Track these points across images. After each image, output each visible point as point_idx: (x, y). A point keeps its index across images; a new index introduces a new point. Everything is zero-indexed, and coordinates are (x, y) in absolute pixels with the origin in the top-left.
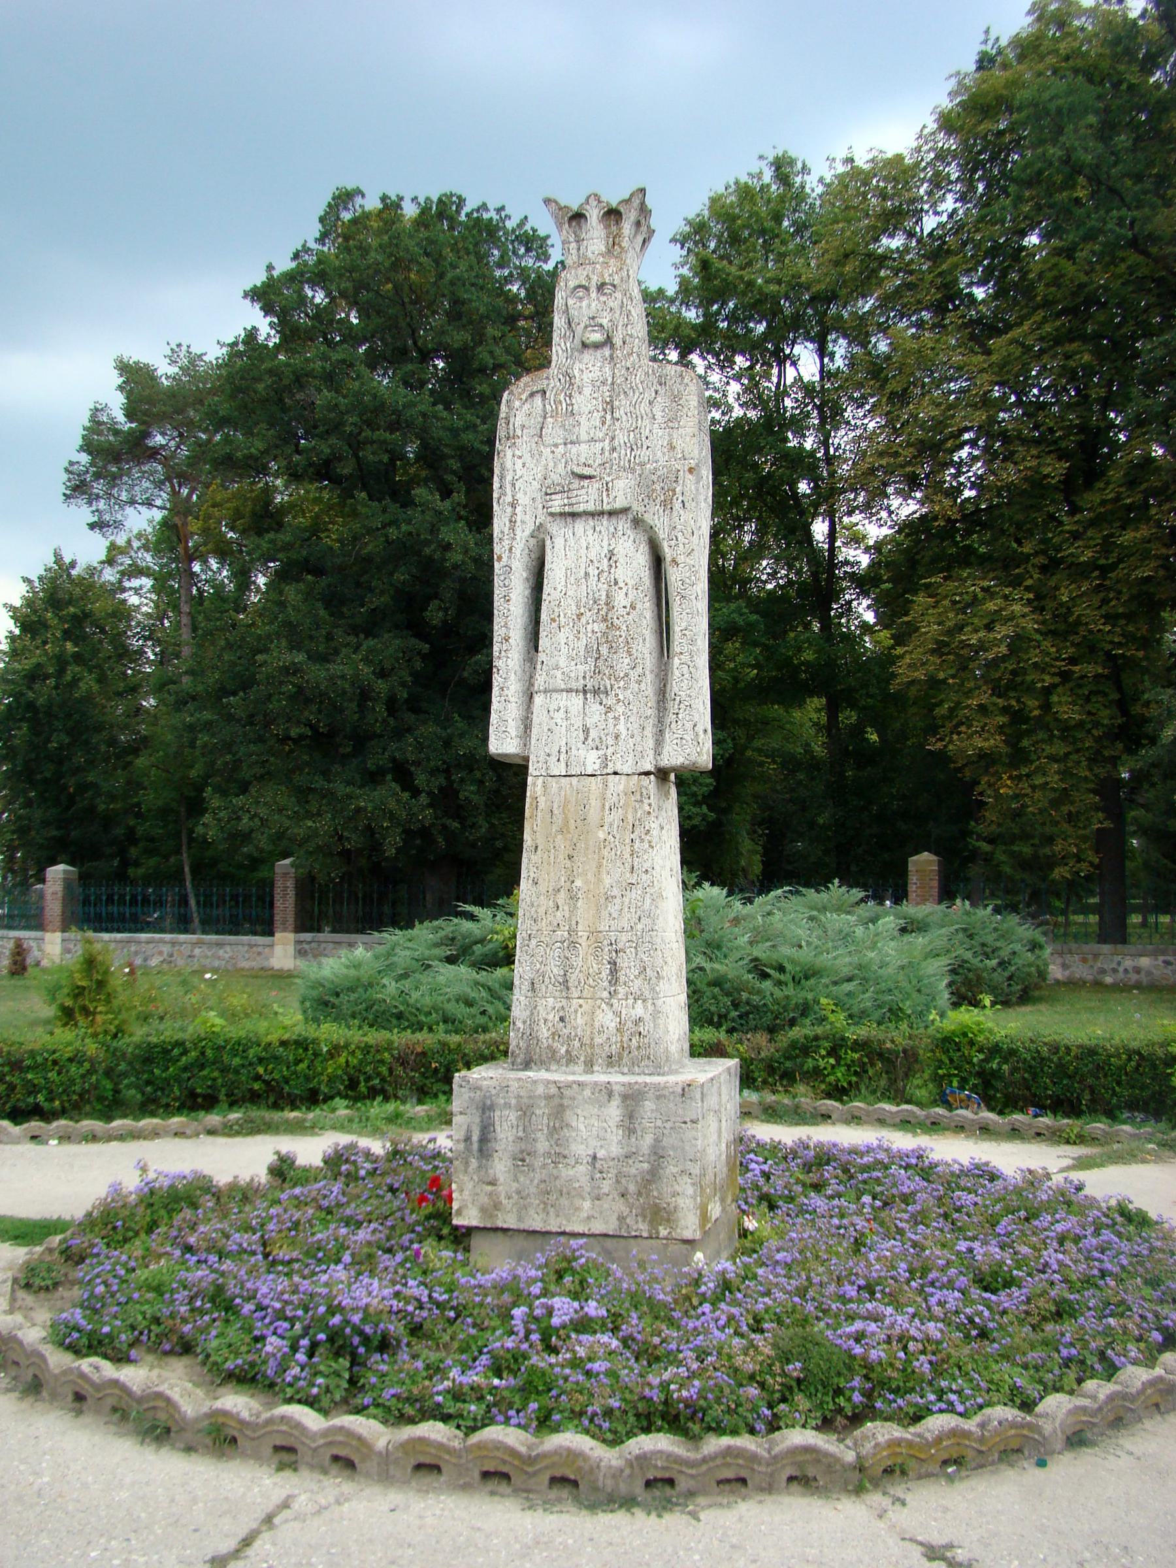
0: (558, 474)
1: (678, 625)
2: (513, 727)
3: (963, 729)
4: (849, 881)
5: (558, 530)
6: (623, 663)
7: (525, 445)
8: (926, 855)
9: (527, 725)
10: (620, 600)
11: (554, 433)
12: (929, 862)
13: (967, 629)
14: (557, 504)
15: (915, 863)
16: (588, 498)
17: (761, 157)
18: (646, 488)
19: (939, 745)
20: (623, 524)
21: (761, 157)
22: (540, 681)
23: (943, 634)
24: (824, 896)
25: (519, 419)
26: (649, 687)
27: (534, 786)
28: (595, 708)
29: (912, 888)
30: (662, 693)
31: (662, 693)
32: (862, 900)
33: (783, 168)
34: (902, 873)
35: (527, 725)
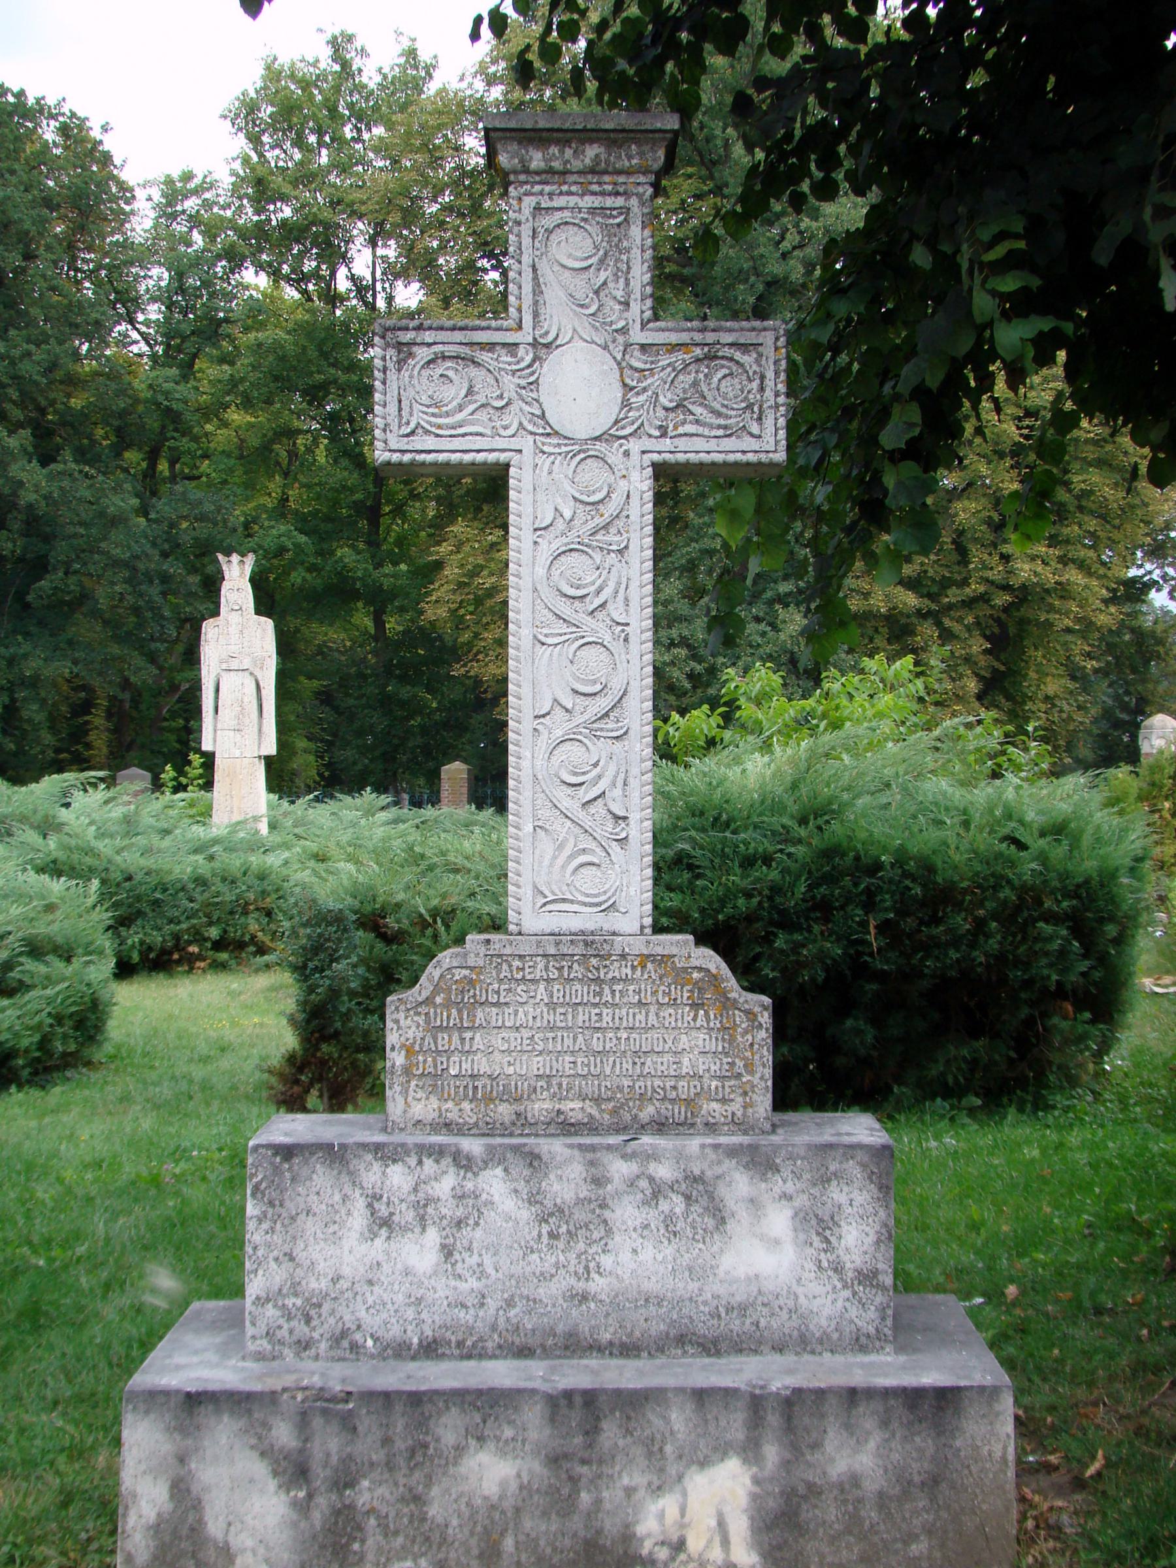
0: (224, 656)
1: (264, 729)
2: (211, 742)
3: (480, 657)
4: (380, 789)
5: (223, 674)
6: (247, 721)
7: (212, 643)
8: (457, 765)
9: (215, 741)
10: (246, 700)
11: (222, 641)
12: (458, 771)
13: (485, 573)
14: (224, 666)
15: (447, 771)
16: (234, 665)
17: (320, 30)
18: (254, 662)
19: (463, 671)
20: (247, 674)
21: (320, 30)
22: (219, 726)
23: (464, 575)
24: (358, 801)
25: (210, 636)
26: (256, 729)
27: (218, 761)
28: (238, 735)
29: (444, 794)
30: (260, 730)
31: (260, 730)
32: (143, 791)
33: (339, 45)
34: (434, 777)
35: (215, 741)
